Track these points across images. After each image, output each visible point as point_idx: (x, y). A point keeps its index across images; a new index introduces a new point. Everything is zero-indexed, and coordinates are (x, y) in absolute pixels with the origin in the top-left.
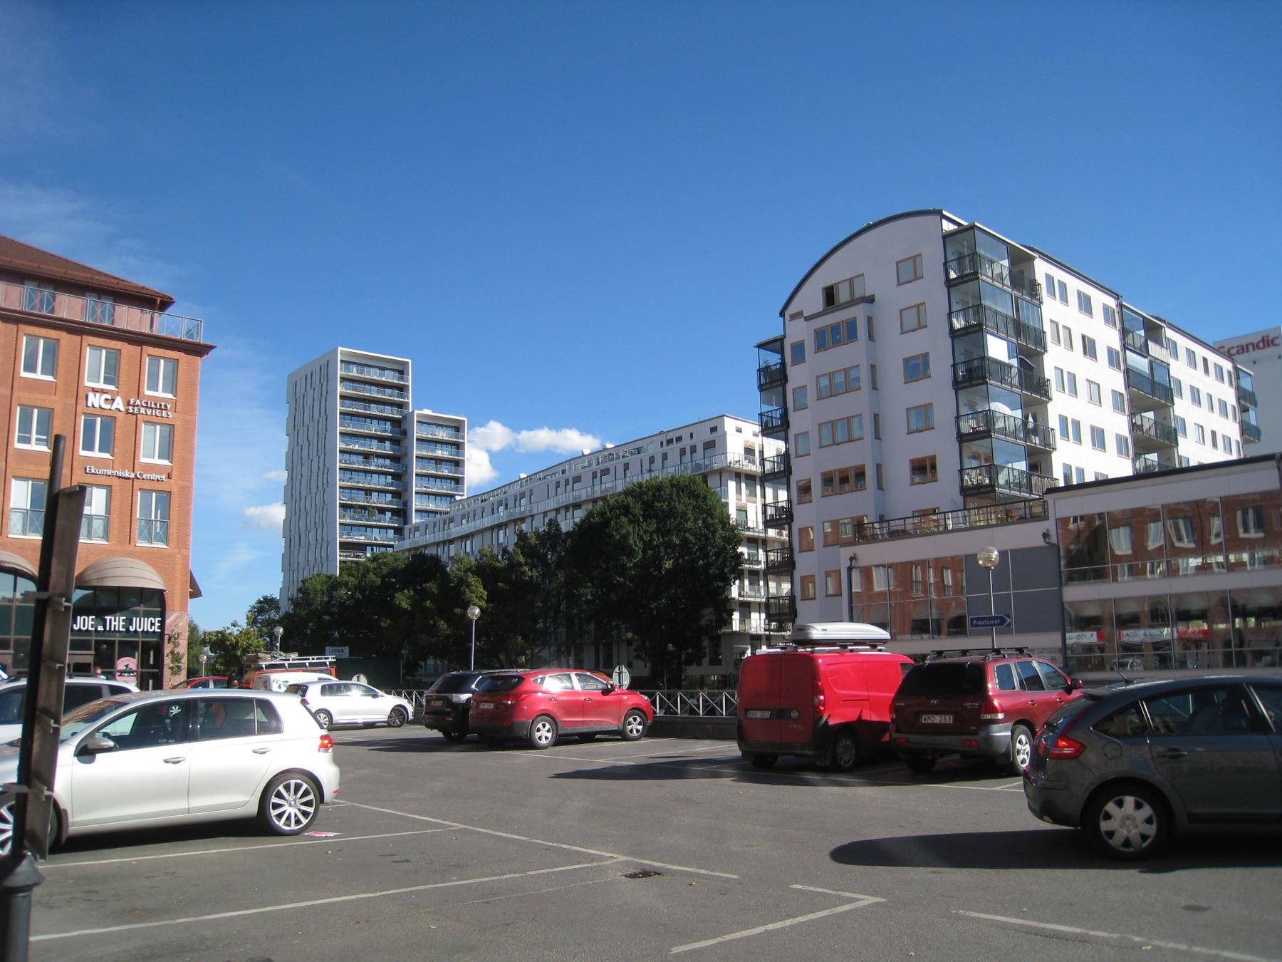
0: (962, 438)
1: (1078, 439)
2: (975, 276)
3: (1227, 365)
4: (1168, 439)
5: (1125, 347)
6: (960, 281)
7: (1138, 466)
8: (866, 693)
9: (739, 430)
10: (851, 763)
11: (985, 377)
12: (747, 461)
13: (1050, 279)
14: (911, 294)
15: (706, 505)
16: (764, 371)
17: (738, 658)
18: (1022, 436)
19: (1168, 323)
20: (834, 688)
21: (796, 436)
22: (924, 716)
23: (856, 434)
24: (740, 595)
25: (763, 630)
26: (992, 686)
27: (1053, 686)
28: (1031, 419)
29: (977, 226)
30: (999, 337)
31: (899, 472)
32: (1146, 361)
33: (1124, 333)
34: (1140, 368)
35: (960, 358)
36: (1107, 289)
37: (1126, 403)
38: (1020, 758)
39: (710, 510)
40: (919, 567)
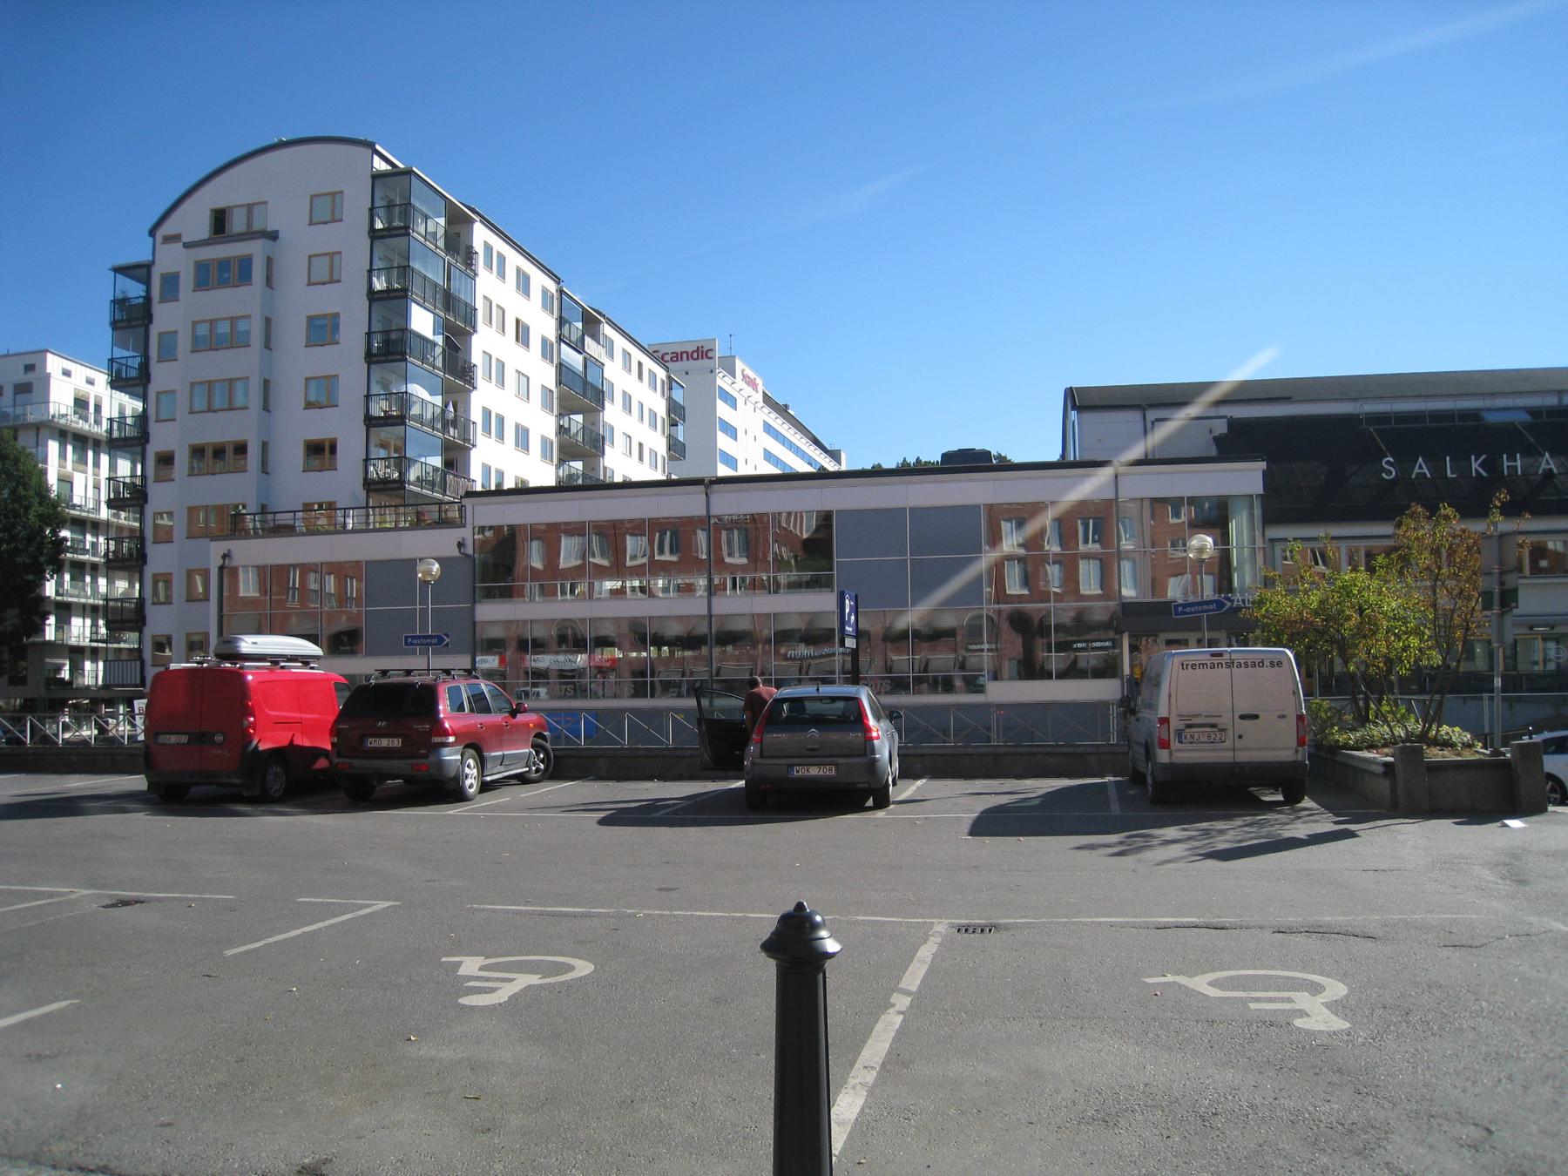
0: (370, 421)
1: (501, 436)
2: (405, 231)
3: (661, 374)
4: (596, 447)
5: (560, 339)
6: (386, 233)
7: (561, 473)
8: (298, 715)
9: (67, 373)
10: (281, 791)
11: (405, 353)
12: (77, 416)
13: (488, 248)
14: (326, 238)
15: (17, 470)
16: (120, 303)
17: (52, 676)
18: (439, 426)
19: (608, 318)
20: (266, 710)
21: (158, 394)
22: (370, 740)
23: (239, 401)
24: (57, 593)
25: (87, 640)
26: (444, 708)
27: (500, 710)
28: (451, 408)
29: (415, 173)
30: (425, 308)
31: (290, 455)
32: (580, 358)
33: (561, 322)
34: (573, 364)
35: (377, 327)
36: (549, 271)
37: (555, 401)
38: (468, 782)
39: (22, 477)
40: (354, 580)
